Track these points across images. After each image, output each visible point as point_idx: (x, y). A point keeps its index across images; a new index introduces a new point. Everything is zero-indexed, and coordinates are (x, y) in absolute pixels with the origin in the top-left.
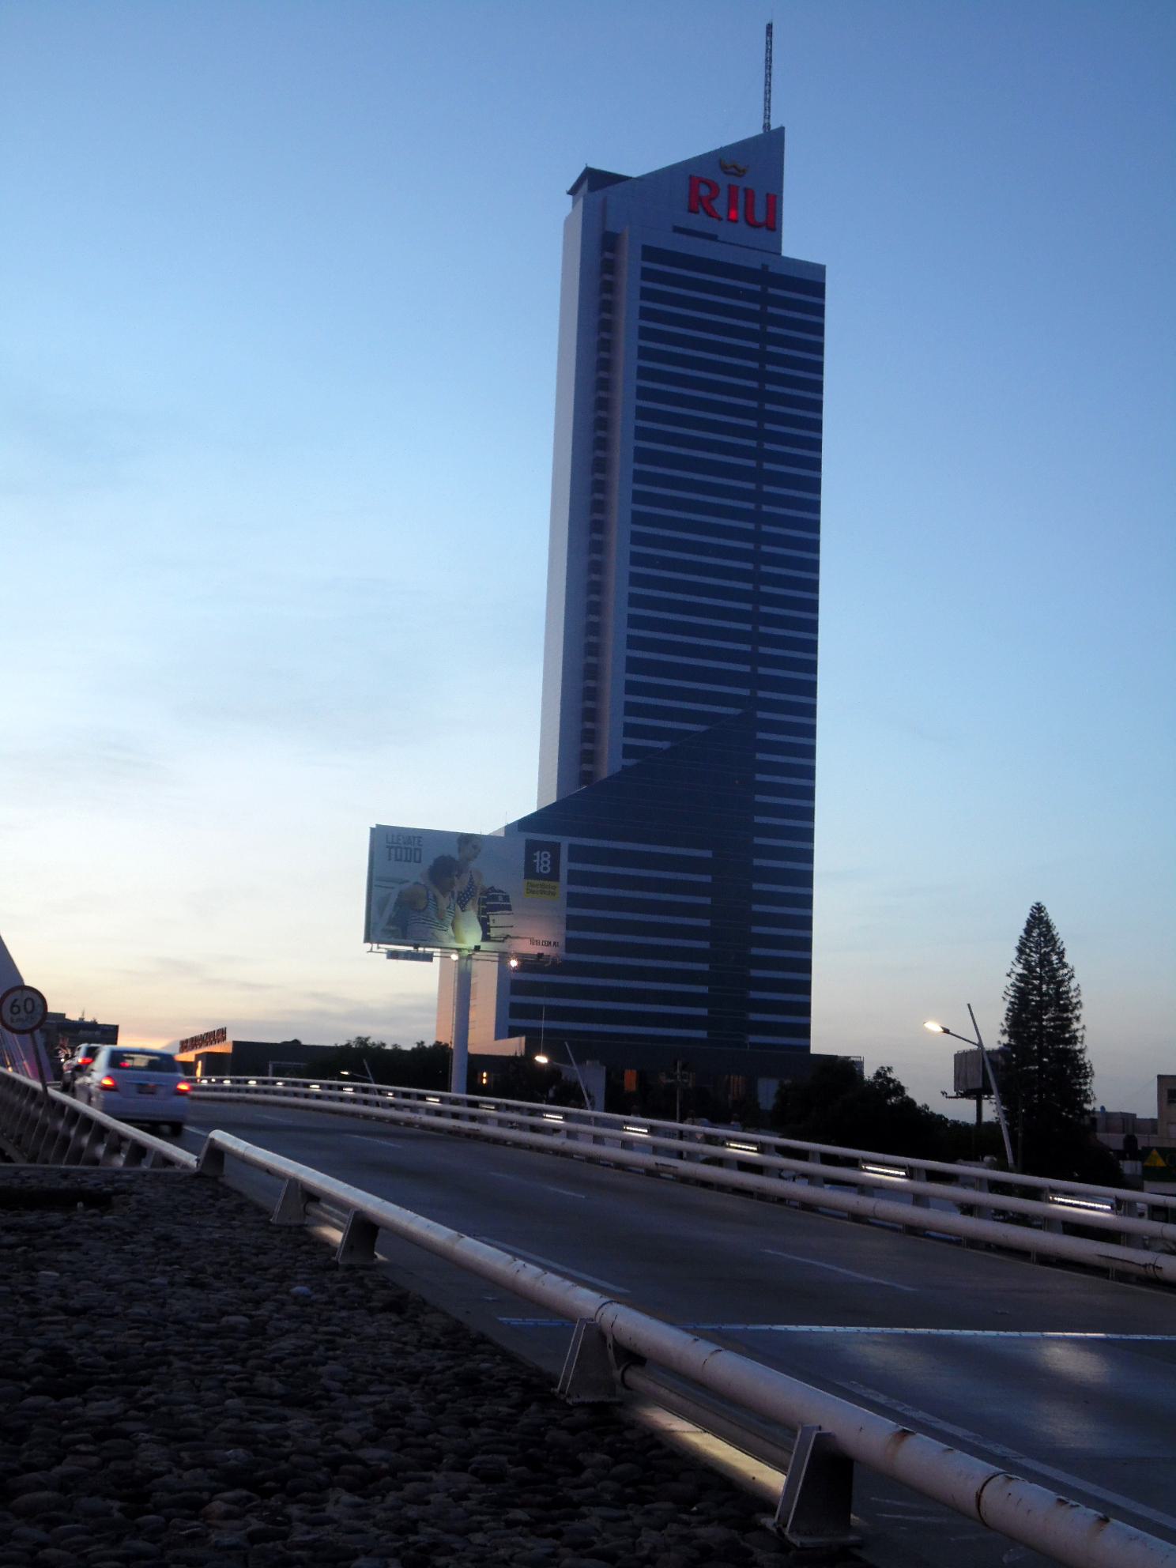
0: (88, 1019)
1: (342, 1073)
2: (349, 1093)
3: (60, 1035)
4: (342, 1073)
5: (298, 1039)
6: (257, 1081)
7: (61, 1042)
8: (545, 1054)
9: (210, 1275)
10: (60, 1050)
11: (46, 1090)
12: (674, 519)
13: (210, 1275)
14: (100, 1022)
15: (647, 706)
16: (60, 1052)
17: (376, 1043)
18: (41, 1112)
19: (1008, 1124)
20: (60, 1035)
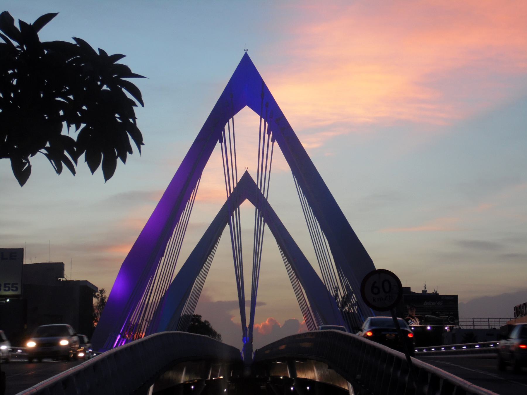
0: (430, 291)
1: (78, 113)
2: (443, 350)
3: (408, 307)
4: (78, 113)
5: (221, 335)
6: (466, 346)
7: (409, 312)
8: (18, 91)
9: (246, 52)
10: (409, 319)
11: (409, 359)
12: (234, 249)
13: (246, 52)
14: (440, 293)
15: (235, 254)
16: (410, 321)
17: (281, 324)
18: (407, 378)
19: (30, 155)
20: (408, 307)
